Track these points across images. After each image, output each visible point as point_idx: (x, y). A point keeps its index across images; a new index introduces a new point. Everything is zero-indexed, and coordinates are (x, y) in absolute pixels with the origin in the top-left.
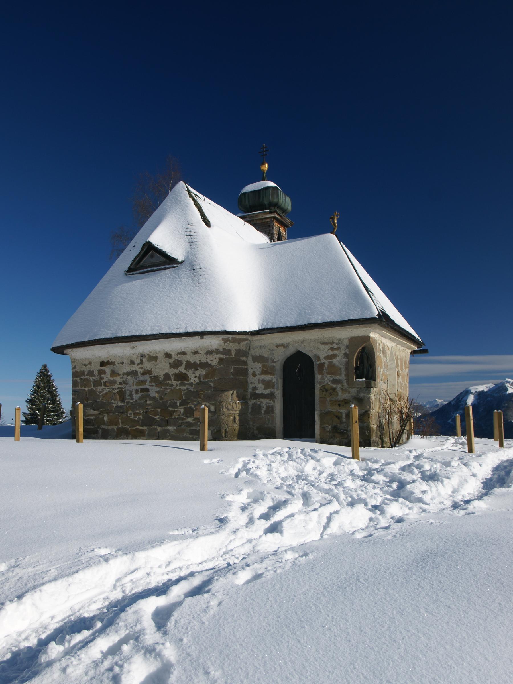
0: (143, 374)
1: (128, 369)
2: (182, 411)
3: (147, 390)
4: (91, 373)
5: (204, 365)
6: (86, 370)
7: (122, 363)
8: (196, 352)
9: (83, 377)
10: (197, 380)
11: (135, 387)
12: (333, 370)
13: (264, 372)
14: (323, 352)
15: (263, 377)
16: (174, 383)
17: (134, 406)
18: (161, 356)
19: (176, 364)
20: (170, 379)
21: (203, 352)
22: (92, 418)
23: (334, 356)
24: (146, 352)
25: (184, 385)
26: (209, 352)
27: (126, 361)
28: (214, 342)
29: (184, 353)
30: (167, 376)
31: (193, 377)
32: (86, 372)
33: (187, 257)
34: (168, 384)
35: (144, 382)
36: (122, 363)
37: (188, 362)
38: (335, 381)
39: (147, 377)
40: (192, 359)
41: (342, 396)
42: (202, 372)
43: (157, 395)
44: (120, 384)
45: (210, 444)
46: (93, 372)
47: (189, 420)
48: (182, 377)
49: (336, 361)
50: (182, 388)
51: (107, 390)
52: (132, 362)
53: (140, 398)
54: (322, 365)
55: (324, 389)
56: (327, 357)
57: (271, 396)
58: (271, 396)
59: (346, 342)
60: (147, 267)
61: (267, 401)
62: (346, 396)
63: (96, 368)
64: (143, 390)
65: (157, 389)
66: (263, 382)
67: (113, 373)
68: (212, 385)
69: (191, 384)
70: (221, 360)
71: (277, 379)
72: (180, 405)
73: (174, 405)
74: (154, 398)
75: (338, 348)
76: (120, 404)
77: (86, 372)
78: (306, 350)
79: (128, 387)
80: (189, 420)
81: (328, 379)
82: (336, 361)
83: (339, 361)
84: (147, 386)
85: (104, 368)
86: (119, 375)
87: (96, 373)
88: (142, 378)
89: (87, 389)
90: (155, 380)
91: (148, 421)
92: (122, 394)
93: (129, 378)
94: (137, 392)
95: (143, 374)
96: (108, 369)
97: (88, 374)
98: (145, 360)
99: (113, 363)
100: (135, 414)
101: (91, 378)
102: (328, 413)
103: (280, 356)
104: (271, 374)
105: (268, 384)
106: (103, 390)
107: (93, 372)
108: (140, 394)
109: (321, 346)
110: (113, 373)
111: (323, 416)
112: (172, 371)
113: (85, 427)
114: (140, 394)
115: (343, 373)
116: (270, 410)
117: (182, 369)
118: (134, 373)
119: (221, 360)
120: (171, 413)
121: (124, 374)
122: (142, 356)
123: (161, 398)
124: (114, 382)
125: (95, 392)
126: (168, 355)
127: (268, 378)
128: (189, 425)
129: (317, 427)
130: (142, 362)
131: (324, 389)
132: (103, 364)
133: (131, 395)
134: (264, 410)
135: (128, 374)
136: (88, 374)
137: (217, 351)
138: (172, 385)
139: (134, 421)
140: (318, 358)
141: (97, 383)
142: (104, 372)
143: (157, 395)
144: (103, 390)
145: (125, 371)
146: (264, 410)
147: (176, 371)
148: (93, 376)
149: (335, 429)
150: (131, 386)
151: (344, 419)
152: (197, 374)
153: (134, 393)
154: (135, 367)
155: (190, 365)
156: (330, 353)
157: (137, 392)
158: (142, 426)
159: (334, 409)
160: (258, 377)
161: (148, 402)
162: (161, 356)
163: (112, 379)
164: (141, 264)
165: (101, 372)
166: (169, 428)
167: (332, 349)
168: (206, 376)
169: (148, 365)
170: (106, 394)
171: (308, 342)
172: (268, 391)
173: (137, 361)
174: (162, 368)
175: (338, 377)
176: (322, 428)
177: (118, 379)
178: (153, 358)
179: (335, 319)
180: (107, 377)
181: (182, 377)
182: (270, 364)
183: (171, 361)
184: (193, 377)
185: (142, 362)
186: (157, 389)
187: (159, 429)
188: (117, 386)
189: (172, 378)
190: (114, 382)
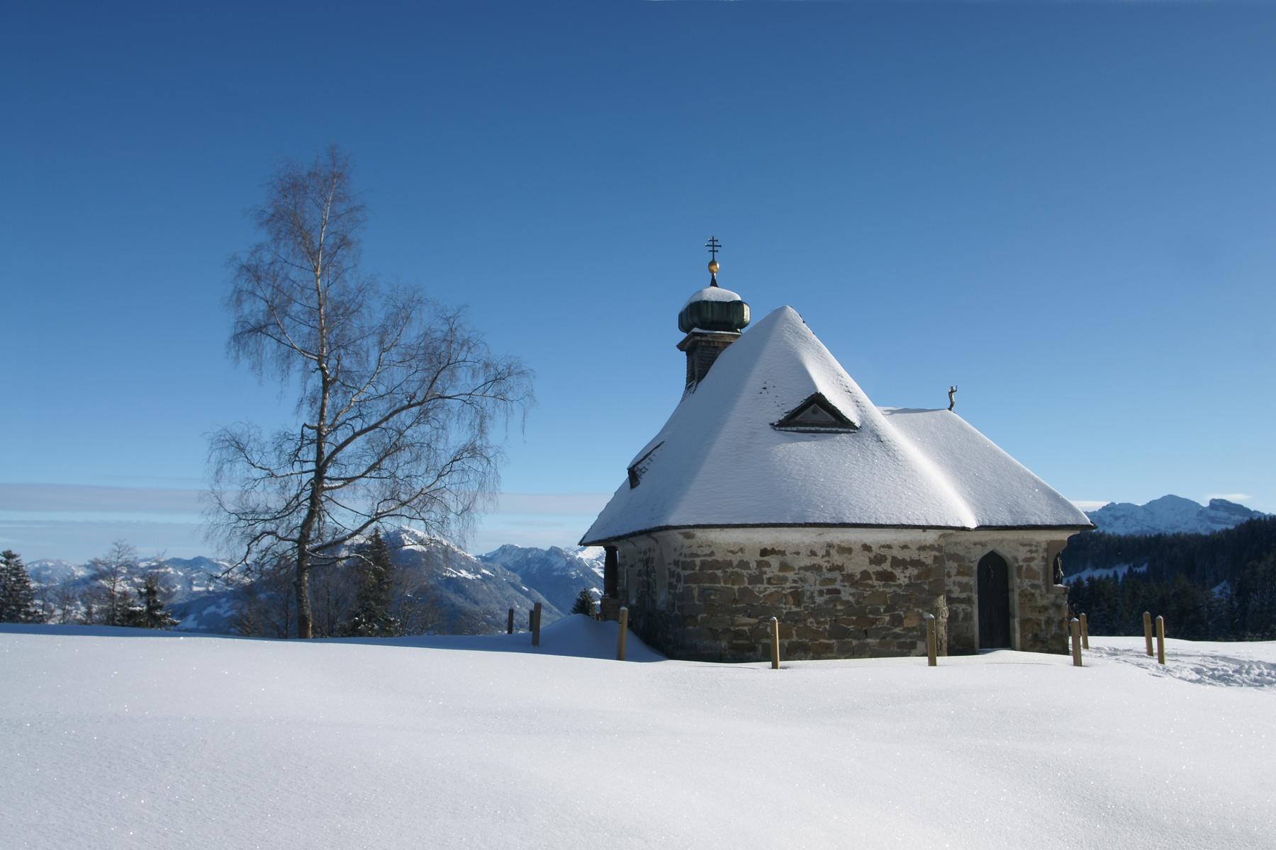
0: (830, 570)
1: (807, 561)
2: (887, 618)
3: (838, 592)
4: (744, 564)
5: (915, 563)
6: (736, 559)
7: (798, 553)
8: (905, 547)
9: (730, 570)
10: (907, 581)
11: (819, 587)
12: (1031, 574)
13: (959, 573)
14: (1022, 553)
15: (959, 579)
16: (876, 583)
17: (817, 612)
18: (857, 548)
19: (879, 560)
20: (870, 578)
21: (914, 547)
22: (746, 628)
23: (1032, 559)
24: (836, 541)
25: (890, 586)
26: (922, 548)
27: (803, 551)
28: (931, 537)
29: (889, 547)
30: (865, 575)
31: (902, 577)
32: (735, 563)
33: (863, 422)
34: (867, 585)
35: (833, 581)
36: (798, 553)
37: (894, 558)
38: (1033, 586)
39: (836, 574)
40: (900, 555)
41: (1041, 602)
42: (912, 571)
43: (851, 598)
44: (795, 581)
45: (780, 663)
46: (748, 563)
47: (898, 630)
48: (887, 577)
49: (1033, 565)
50: (887, 590)
51: (772, 589)
52: (813, 553)
53: (826, 602)
54: (1020, 568)
55: (1023, 594)
56: (1026, 560)
57: (968, 601)
58: (968, 601)
59: (1044, 545)
60: (806, 425)
61: (964, 606)
62: (1045, 602)
63: (753, 558)
64: (829, 592)
65: (853, 591)
66: (960, 584)
67: (784, 567)
68: (926, 587)
69: (899, 586)
70: (935, 557)
71: (973, 581)
72: (885, 611)
73: (877, 612)
74: (848, 602)
75: (1036, 551)
76: (794, 609)
77: (735, 563)
78: (1004, 552)
79: (807, 587)
80: (898, 630)
81: (1027, 582)
82: (1033, 565)
83: (1037, 564)
84: (837, 586)
85: (766, 558)
86: (793, 569)
87: (753, 565)
88: (829, 575)
89: (736, 587)
90: (849, 577)
91: (839, 632)
92: (797, 596)
93: (808, 574)
94: (821, 593)
95: (830, 570)
96: (774, 561)
97: (738, 566)
98: (833, 552)
99: (783, 553)
100: (818, 623)
101: (744, 572)
102: (1029, 620)
103: (978, 554)
104: (968, 575)
105: (964, 587)
106: (766, 589)
107: (748, 563)
108: (826, 597)
109: (1021, 548)
110: (784, 567)
111: (1024, 622)
112: (873, 569)
113: (977, 645)
114: (826, 597)
115: (1042, 577)
116: (968, 617)
117: (886, 566)
118: (816, 568)
119: (935, 557)
120: (873, 622)
121: (800, 568)
122: (830, 546)
123: (858, 602)
124: (786, 579)
125: (751, 592)
126: (866, 548)
127: (965, 579)
128: (897, 636)
129: (1018, 636)
130: (828, 554)
131: (1023, 594)
132: (764, 552)
133: (812, 597)
134: (961, 616)
135: (806, 569)
136: (738, 566)
137: (932, 548)
138: (873, 587)
139: (817, 632)
140: (1016, 560)
141: (756, 580)
142: (768, 565)
143: (851, 598)
144: (766, 589)
145: (802, 565)
146: (961, 616)
147: (879, 568)
148: (749, 568)
149: (1036, 636)
150: (813, 584)
151: (1043, 627)
152: (907, 573)
153: (816, 594)
154: (817, 560)
155: (896, 562)
156: (1029, 555)
157: (821, 593)
158: (829, 638)
159: (1034, 616)
160: (953, 578)
161: (839, 607)
162: (857, 548)
163: (781, 574)
164: (798, 418)
165: (760, 564)
166: (869, 640)
167: (1031, 551)
168: (918, 577)
169: (837, 559)
170: (771, 594)
171: (1008, 546)
172: (964, 595)
173: (822, 552)
174: (857, 564)
175: (1036, 582)
176: (1023, 637)
177: (791, 575)
178: (846, 550)
179: (1054, 523)
180: (773, 569)
181: (887, 577)
182: (967, 564)
183: (872, 555)
184: (902, 577)
185: (828, 554)
186: (853, 591)
187: (855, 642)
188: (788, 585)
189: (874, 577)
190: (786, 579)
